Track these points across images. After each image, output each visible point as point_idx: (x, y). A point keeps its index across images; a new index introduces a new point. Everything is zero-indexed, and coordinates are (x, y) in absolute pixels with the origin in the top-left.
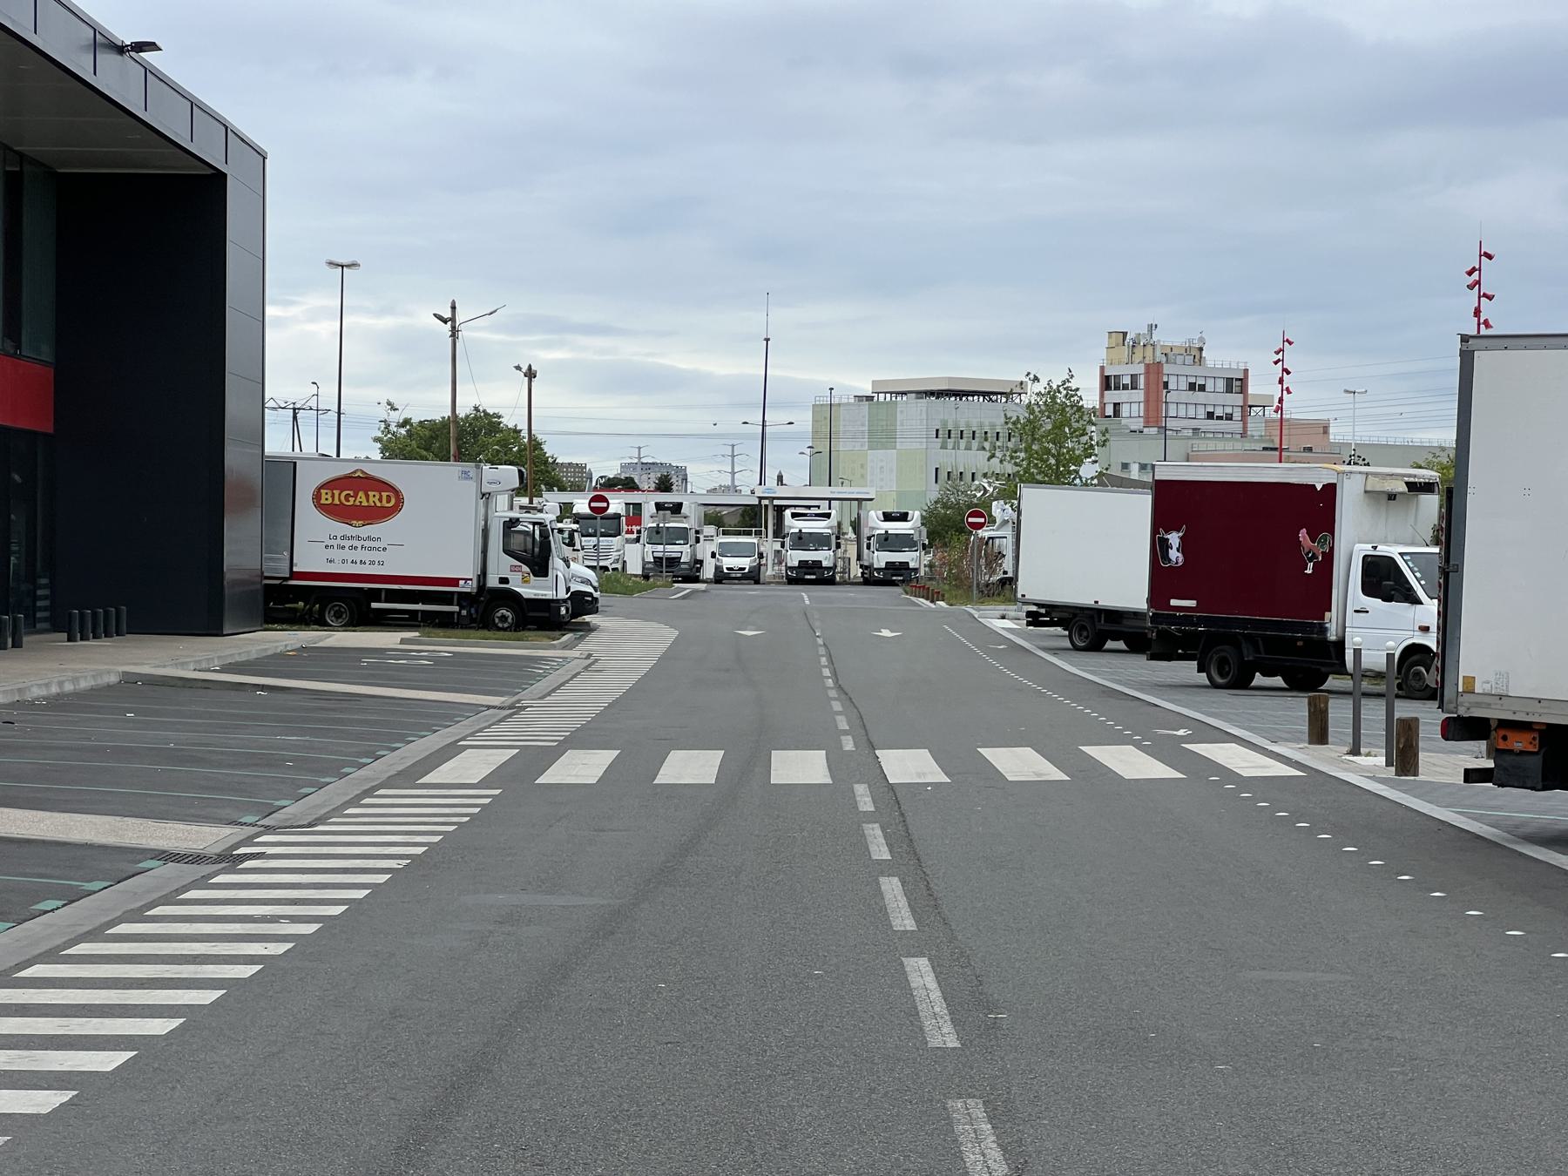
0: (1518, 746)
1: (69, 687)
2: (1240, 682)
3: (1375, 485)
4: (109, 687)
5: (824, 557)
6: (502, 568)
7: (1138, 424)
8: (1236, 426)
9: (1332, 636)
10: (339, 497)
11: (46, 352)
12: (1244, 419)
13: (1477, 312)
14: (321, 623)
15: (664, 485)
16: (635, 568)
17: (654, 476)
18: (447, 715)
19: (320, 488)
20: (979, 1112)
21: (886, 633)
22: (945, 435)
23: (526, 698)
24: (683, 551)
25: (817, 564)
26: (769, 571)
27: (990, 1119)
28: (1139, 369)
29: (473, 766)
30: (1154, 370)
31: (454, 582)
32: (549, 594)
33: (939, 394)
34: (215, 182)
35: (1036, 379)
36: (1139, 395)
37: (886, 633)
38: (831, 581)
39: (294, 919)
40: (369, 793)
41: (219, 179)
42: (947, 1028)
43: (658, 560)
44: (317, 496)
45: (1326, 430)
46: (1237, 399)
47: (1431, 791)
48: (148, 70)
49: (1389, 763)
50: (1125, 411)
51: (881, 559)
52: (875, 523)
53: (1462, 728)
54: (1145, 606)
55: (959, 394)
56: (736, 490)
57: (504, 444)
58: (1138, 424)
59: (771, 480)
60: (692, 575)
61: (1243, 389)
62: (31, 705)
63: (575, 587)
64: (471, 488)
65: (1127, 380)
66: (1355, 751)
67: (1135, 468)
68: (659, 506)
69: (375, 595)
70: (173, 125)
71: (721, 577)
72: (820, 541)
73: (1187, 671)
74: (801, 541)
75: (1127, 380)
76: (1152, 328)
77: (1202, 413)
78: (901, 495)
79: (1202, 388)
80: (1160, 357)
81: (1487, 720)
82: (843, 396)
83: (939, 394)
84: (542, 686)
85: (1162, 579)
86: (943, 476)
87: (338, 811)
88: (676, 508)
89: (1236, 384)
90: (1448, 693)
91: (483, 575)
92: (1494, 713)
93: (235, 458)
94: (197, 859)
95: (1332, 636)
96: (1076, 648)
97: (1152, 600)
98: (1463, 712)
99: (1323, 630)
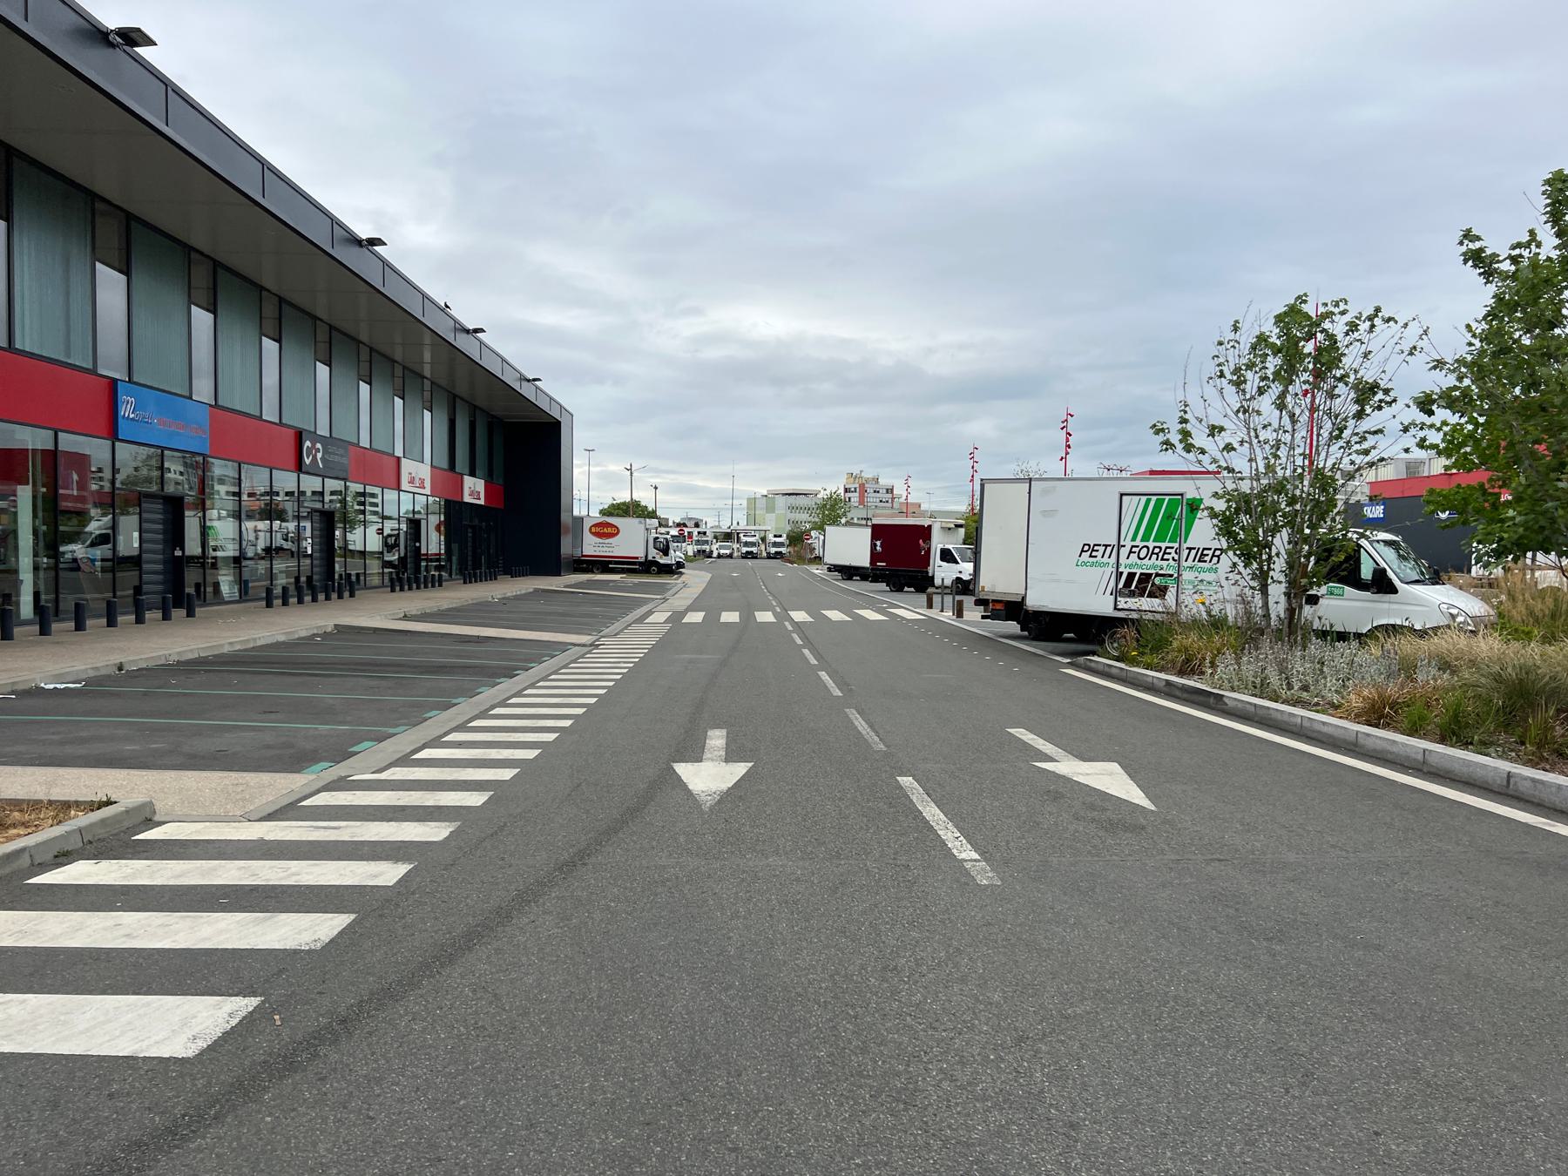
0: (998, 608)
1: (518, 593)
2: (899, 589)
3: (944, 525)
4: (530, 593)
5: (754, 550)
6: (654, 554)
7: (857, 504)
8: (889, 505)
9: (930, 575)
10: (598, 530)
11: (501, 482)
12: (892, 503)
13: (973, 467)
14: (592, 572)
15: (697, 525)
16: (690, 553)
17: (693, 522)
18: (645, 602)
19: (593, 526)
20: (854, 712)
21: (780, 574)
22: (792, 508)
23: (667, 595)
24: (707, 548)
25: (752, 552)
26: (735, 554)
27: (859, 714)
28: (857, 486)
29: (659, 617)
30: (862, 486)
31: (637, 558)
32: (669, 562)
33: (790, 494)
34: (558, 424)
35: (825, 490)
36: (857, 494)
37: (780, 574)
38: (756, 558)
39: (625, 662)
40: (629, 625)
41: (559, 423)
42: (837, 691)
43: (699, 551)
44: (590, 529)
45: (920, 506)
46: (890, 495)
47: (967, 623)
48: (537, 387)
49: (954, 614)
50: (852, 500)
51: (773, 550)
52: (771, 538)
53: (979, 602)
54: (868, 565)
55: (797, 494)
56: (719, 527)
57: (643, 511)
58: (857, 504)
59: (735, 523)
60: (710, 556)
61: (892, 492)
62: (508, 598)
63: (677, 560)
64: (643, 526)
65: (853, 489)
66: (942, 611)
67: (855, 519)
68: (699, 533)
69: (611, 562)
70: (543, 404)
71: (719, 556)
72: (753, 544)
73: (883, 586)
74: (746, 544)
75: (853, 489)
76: (861, 471)
77: (878, 500)
78: (777, 529)
79: (878, 492)
80: (864, 482)
81: (988, 600)
82: (758, 496)
83: (790, 494)
84: (671, 592)
85: (875, 556)
86: (791, 522)
87: (622, 631)
88: (705, 533)
89: (890, 490)
90: (976, 592)
91: (646, 556)
92: (991, 597)
93: (564, 517)
94: (584, 645)
95: (930, 575)
96: (844, 579)
97: (871, 563)
98: (981, 597)
99: (927, 573)
